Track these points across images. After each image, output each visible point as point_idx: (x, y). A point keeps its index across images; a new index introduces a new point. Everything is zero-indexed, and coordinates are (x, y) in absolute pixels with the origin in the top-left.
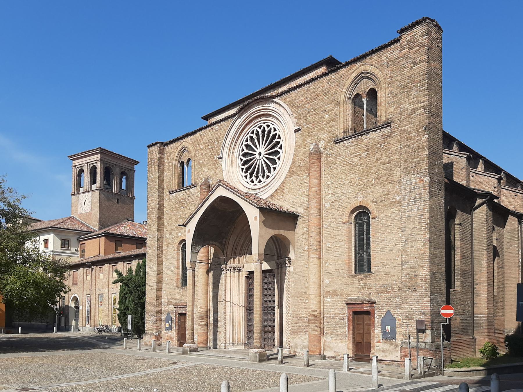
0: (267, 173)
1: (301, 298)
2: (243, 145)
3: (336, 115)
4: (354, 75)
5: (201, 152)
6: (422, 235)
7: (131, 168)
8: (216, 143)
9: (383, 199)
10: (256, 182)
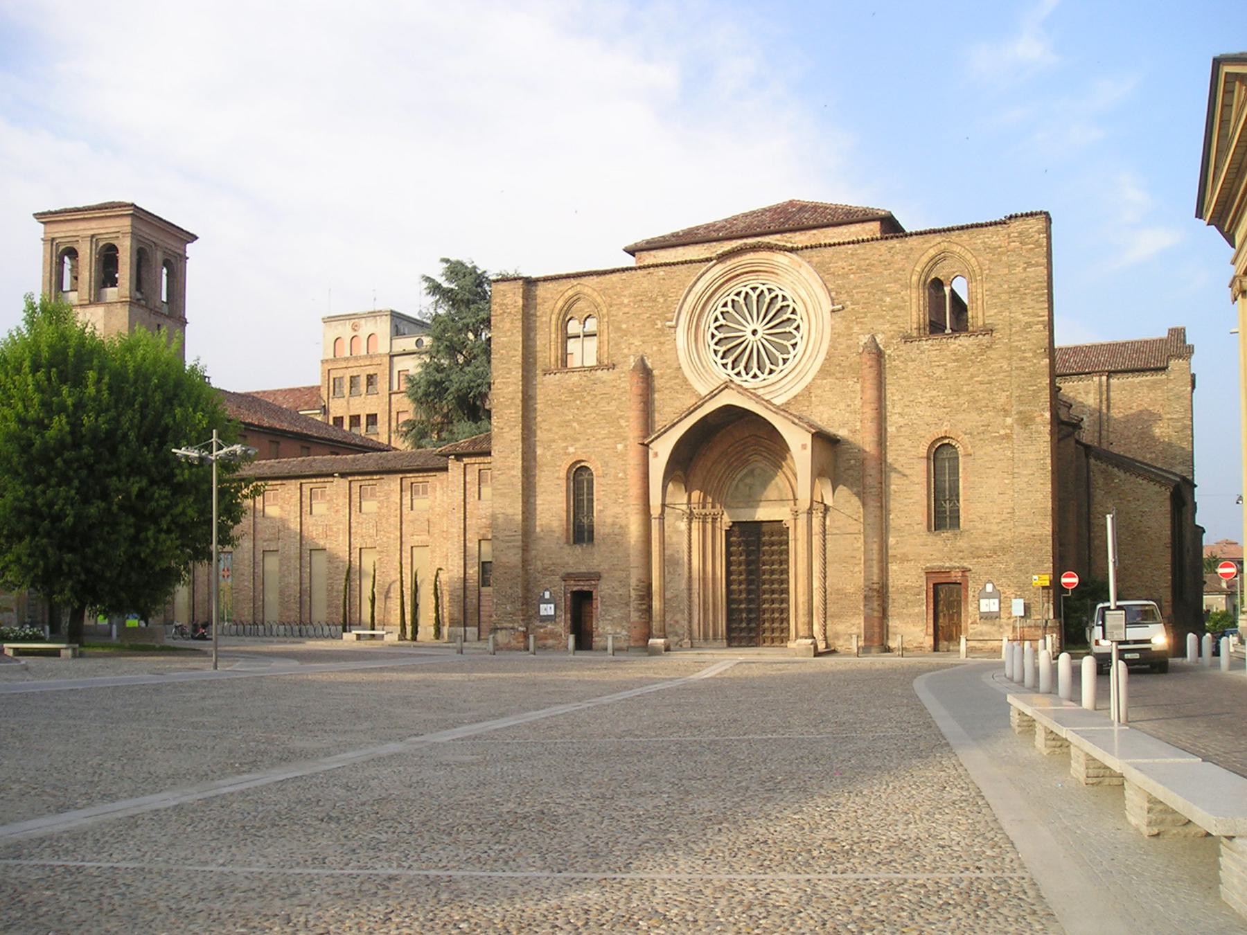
4: (932, 252)
5: (626, 310)
8: (661, 300)
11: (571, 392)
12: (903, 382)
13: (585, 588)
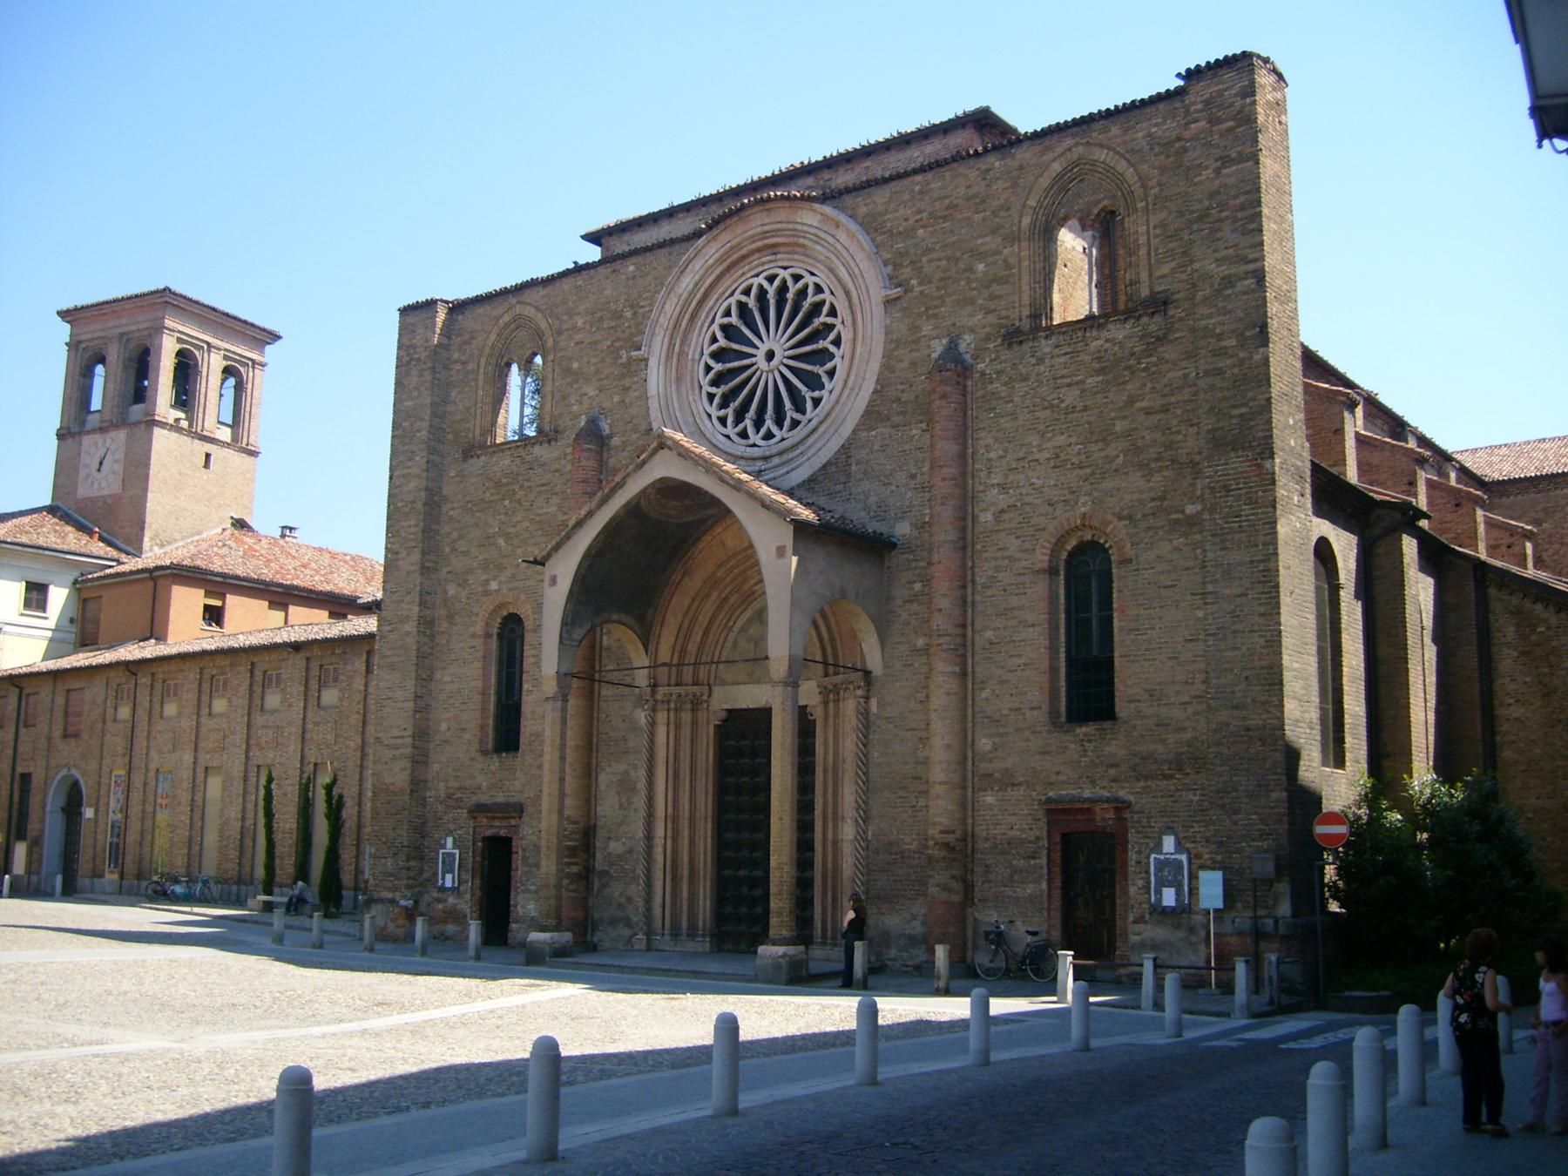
0: (790, 413)
1: (902, 793)
2: (715, 327)
3: (1008, 266)
4: (1057, 167)
5: (579, 337)
6: (1261, 615)
8: (628, 314)
9: (1148, 510)
10: (755, 438)
11: (498, 484)
12: (1005, 423)
13: (503, 833)
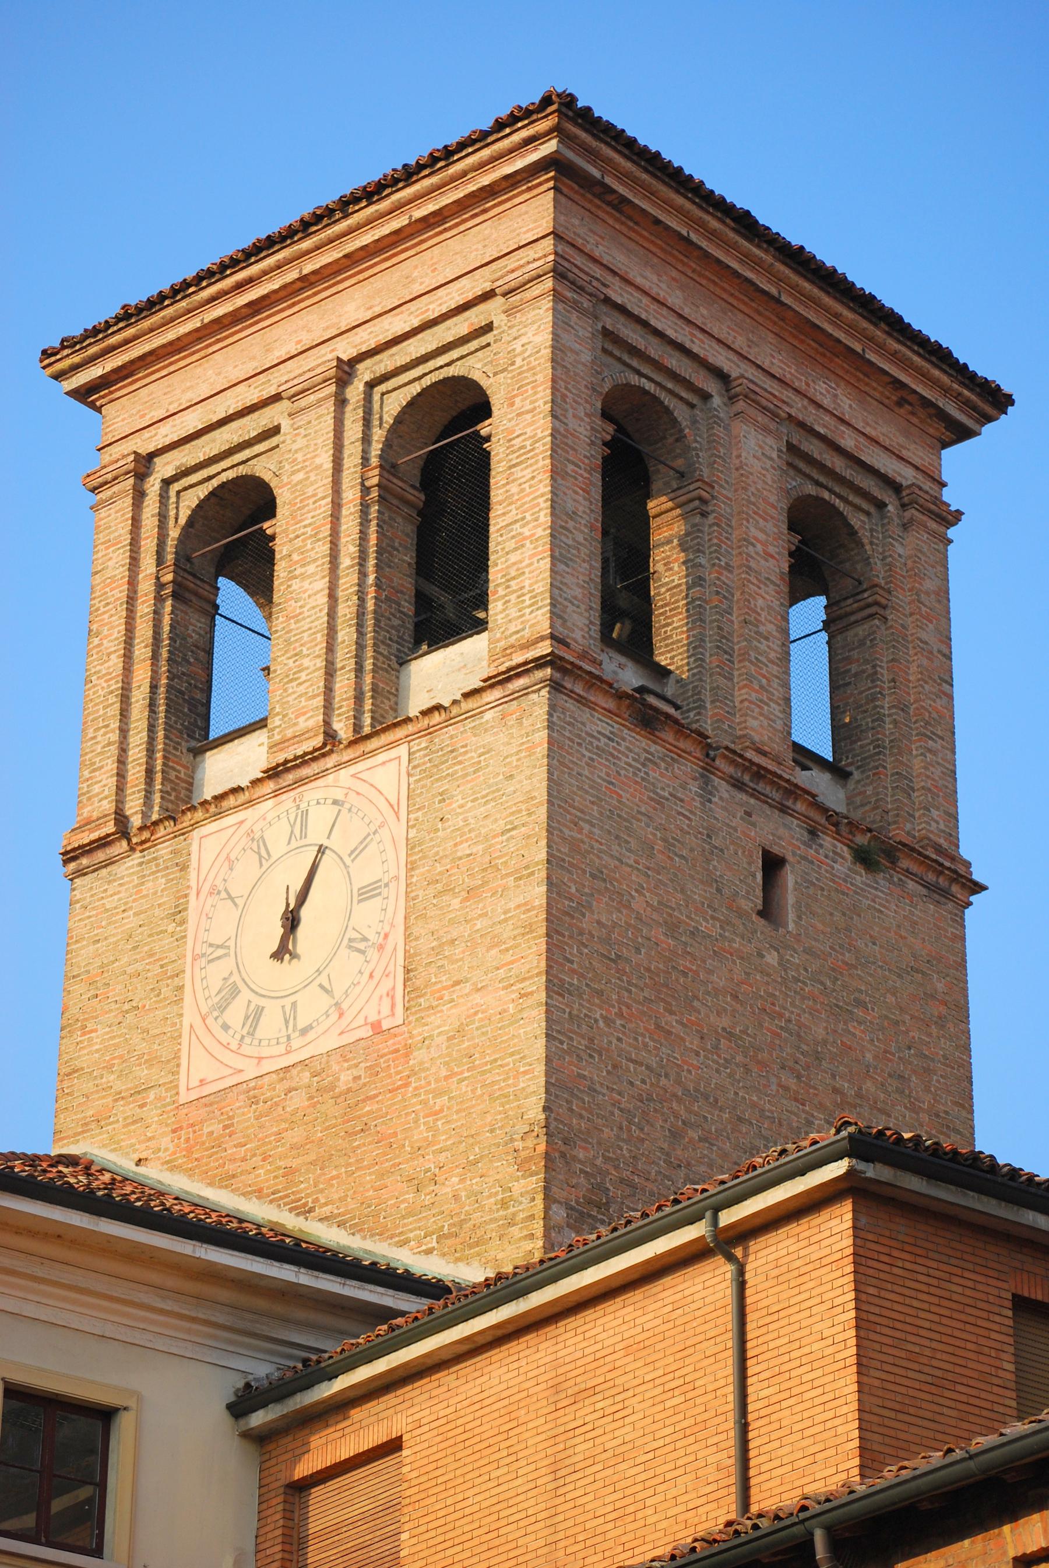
7: (906, 475)
